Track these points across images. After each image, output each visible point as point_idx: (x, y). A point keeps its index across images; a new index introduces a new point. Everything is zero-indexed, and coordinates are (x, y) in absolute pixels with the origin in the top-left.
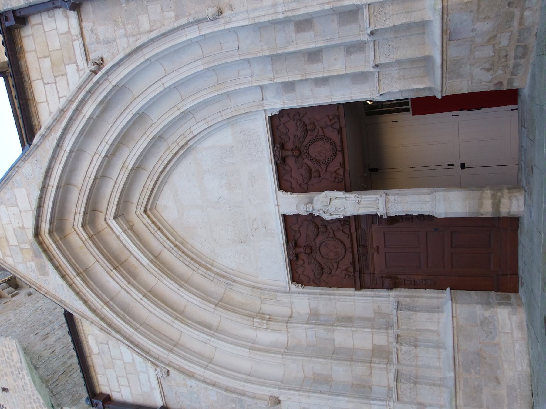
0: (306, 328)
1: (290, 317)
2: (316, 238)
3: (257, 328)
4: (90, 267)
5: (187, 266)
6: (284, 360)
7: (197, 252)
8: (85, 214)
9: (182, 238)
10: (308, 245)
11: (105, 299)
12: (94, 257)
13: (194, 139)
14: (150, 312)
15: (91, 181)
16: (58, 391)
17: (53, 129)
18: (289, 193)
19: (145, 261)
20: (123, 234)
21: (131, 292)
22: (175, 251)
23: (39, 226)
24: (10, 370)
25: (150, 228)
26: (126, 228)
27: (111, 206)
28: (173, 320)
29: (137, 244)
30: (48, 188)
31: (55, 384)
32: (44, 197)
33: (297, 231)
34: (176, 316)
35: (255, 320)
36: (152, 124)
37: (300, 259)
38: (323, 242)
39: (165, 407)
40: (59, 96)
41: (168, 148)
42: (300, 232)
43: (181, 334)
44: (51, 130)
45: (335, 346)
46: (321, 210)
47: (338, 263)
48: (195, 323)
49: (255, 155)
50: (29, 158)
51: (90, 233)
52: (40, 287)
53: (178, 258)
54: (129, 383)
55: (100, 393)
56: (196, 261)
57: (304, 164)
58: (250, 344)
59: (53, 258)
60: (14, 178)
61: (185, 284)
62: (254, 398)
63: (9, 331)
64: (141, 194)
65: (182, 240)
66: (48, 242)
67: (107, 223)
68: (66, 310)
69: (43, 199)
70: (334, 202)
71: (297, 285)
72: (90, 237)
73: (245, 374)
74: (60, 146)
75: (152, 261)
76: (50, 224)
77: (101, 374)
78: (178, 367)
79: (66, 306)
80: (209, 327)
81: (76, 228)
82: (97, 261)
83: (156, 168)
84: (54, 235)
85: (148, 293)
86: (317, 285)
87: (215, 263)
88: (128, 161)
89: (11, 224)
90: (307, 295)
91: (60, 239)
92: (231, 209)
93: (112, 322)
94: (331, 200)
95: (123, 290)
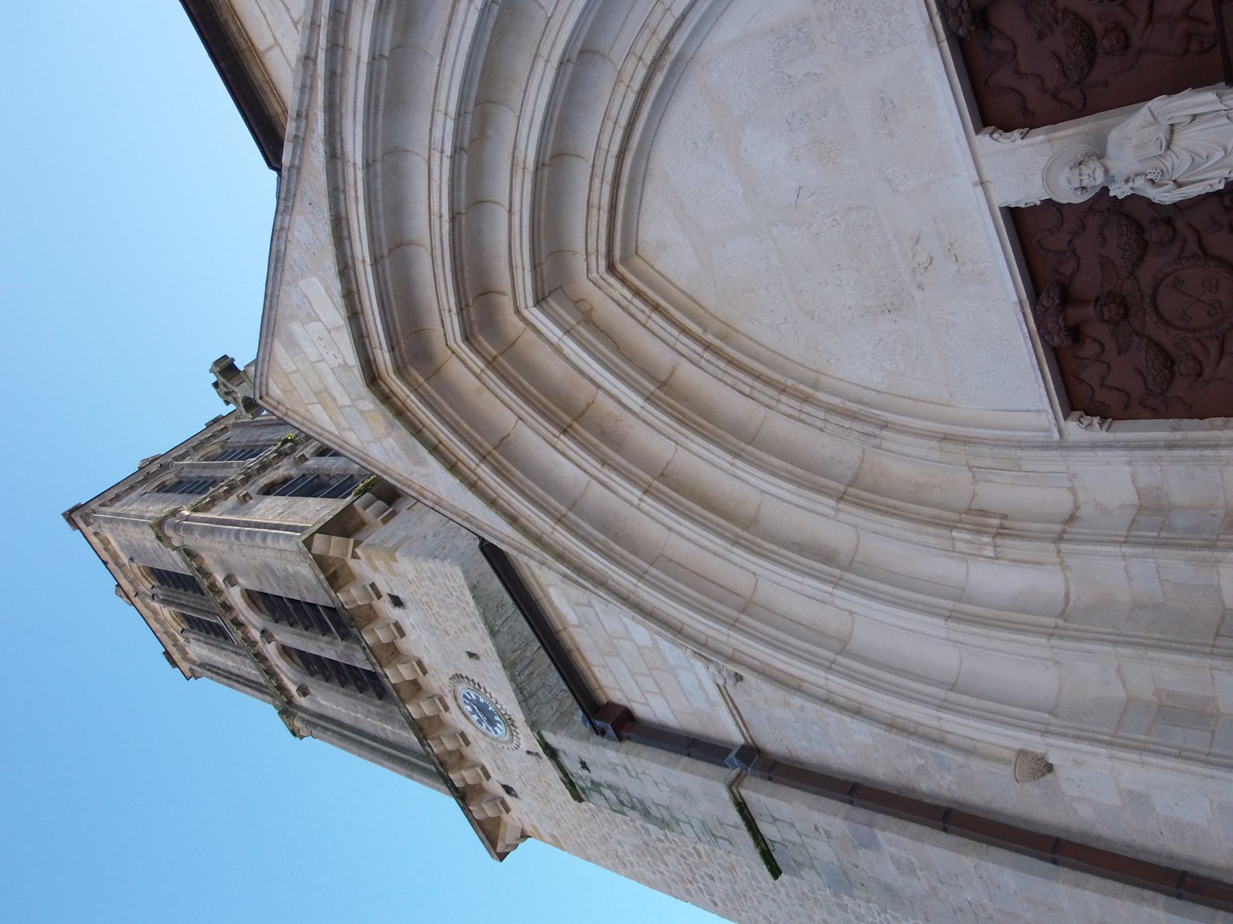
0: (1124, 556)
1: (1071, 519)
2: (1136, 266)
3: (965, 556)
4: (509, 435)
5: (747, 396)
6: (1055, 650)
7: (769, 353)
8: (462, 309)
9: (723, 322)
10: (1109, 292)
11: (556, 510)
12: (511, 410)
13: (682, 29)
14: (669, 529)
15: (446, 227)
16: (533, 689)
17: (310, 115)
18: (1016, 134)
19: (634, 400)
20: (566, 339)
21: (613, 484)
22: (707, 361)
23: (372, 358)
24: (469, 620)
25: (632, 309)
26: (573, 322)
27: (518, 273)
28: (729, 546)
29: (608, 358)
30: (355, 266)
31: (527, 672)
32: (355, 290)
33: (1065, 252)
34: (737, 535)
35: (954, 534)
36: (545, 22)
37: (1088, 340)
38: (1166, 275)
39: (751, 748)
40: (292, 19)
41: (618, 80)
42: (1076, 255)
43: (757, 579)
44: (307, 117)
45: (1224, 605)
46: (1137, 175)
47: (1223, 341)
48: (787, 548)
49: (881, 28)
50: (293, 202)
51: (488, 351)
52: (421, 490)
53: (720, 380)
54: (660, 689)
55: (608, 703)
56: (768, 382)
57: (1060, 15)
58: (949, 604)
59: (421, 426)
60: (288, 257)
61: (749, 448)
62: (971, 752)
63: (448, 547)
64: (587, 226)
65: (724, 327)
66: (401, 392)
67: (524, 319)
68: (483, 539)
69: (356, 296)
70: (1187, 138)
71: (1087, 420)
72: (490, 363)
73: (941, 684)
74: (338, 155)
75: (652, 398)
76: (392, 349)
77: (599, 666)
78: (758, 664)
79: (482, 529)
80: (827, 556)
81: (454, 346)
82: (521, 419)
83: (604, 145)
84: (410, 374)
85: (656, 483)
86: (1155, 414)
87: (824, 379)
88: (522, 146)
89: (324, 360)
90: (1121, 453)
91: (426, 380)
92: (837, 217)
93: (584, 562)
94: (1172, 131)
95: (594, 482)
